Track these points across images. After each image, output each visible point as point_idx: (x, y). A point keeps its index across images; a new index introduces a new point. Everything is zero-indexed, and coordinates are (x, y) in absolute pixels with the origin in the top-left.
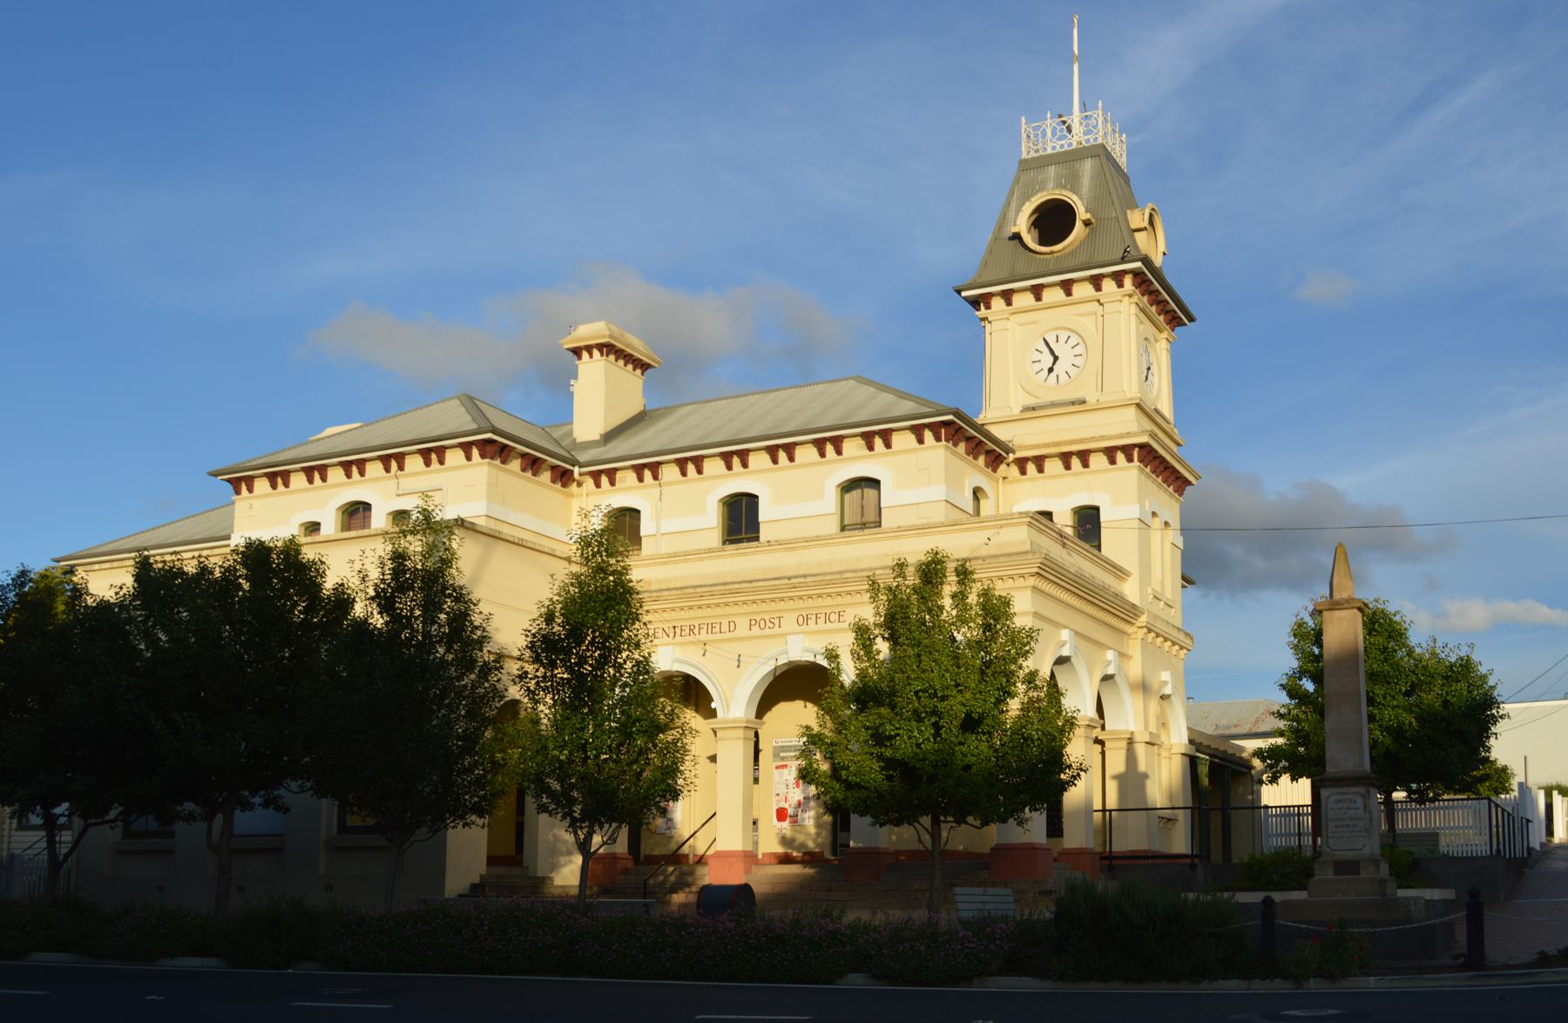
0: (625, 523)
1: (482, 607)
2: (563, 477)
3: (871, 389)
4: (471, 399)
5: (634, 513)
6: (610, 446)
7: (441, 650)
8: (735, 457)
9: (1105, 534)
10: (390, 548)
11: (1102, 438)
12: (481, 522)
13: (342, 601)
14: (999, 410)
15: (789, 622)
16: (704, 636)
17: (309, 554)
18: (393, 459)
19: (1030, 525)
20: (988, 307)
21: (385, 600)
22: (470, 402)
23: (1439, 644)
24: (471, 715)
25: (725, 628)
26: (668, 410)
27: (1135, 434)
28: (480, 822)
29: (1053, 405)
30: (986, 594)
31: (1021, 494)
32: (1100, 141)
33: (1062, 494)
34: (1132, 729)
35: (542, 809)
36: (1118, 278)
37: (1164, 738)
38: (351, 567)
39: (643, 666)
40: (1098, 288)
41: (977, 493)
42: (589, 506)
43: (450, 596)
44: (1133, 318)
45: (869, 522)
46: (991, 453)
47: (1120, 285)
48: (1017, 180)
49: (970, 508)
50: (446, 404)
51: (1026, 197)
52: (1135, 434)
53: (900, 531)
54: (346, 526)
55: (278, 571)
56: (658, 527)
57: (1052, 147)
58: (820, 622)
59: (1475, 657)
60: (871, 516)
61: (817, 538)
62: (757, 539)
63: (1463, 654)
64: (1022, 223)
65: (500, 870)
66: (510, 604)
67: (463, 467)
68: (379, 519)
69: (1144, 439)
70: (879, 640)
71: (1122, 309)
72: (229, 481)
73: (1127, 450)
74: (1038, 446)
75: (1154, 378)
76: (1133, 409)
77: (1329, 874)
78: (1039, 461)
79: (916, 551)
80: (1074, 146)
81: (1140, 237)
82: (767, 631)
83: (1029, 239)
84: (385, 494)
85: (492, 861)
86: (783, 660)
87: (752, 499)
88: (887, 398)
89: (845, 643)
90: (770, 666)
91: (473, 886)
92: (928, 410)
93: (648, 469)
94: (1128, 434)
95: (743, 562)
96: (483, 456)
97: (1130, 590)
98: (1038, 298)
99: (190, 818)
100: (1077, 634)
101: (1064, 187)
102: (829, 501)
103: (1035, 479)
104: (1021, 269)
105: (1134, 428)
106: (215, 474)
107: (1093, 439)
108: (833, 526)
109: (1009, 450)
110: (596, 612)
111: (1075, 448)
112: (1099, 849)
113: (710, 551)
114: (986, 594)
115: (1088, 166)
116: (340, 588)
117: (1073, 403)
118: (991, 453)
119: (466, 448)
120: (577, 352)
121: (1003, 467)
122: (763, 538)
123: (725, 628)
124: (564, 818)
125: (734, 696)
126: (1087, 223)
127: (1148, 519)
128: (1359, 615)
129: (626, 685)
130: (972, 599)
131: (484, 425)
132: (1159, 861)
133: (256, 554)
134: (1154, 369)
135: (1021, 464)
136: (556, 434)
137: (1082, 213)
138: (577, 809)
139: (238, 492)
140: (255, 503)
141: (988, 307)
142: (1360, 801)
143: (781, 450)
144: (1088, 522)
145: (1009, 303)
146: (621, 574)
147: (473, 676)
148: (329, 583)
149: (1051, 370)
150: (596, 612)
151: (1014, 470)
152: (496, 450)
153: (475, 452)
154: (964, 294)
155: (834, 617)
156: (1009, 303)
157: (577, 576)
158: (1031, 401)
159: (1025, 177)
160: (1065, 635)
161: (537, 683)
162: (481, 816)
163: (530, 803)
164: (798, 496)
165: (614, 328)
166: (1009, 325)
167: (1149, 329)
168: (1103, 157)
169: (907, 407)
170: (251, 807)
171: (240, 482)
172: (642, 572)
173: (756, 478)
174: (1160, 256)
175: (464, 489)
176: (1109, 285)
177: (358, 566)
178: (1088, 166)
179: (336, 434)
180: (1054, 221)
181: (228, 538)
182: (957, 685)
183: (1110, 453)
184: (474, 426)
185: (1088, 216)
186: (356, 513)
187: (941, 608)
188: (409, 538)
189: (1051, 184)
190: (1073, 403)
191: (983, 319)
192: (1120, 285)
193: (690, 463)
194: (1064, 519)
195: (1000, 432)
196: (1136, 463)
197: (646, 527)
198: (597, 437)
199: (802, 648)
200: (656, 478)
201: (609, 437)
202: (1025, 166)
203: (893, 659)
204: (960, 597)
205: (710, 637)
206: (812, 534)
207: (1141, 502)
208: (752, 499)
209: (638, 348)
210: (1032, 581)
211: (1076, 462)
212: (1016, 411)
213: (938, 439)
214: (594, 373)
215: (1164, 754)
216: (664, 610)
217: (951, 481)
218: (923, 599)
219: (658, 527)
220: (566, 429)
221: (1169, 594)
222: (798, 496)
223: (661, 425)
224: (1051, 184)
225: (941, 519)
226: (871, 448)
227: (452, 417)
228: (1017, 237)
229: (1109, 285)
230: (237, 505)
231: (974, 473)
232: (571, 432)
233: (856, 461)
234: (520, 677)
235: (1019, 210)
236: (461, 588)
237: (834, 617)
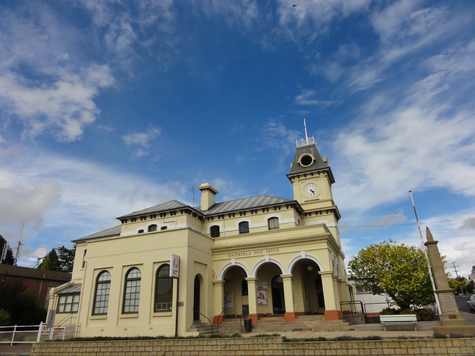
6: (210, 211)
25: (248, 254)
29: (312, 200)
56: (224, 230)
57: (303, 145)
62: (248, 232)
77: (448, 319)
93: (221, 216)
102: (237, 227)
104: (301, 171)
112: (339, 309)
120: (202, 190)
122: (251, 231)
123: (248, 254)
137: (313, 158)
143: (254, 210)
181: (119, 234)
183: (327, 211)
193: (232, 214)
197: (221, 230)
201: (210, 209)
202: (298, 149)
214: (206, 195)
219: (224, 230)
228: (299, 164)
233: (243, 219)
237: (276, 250)
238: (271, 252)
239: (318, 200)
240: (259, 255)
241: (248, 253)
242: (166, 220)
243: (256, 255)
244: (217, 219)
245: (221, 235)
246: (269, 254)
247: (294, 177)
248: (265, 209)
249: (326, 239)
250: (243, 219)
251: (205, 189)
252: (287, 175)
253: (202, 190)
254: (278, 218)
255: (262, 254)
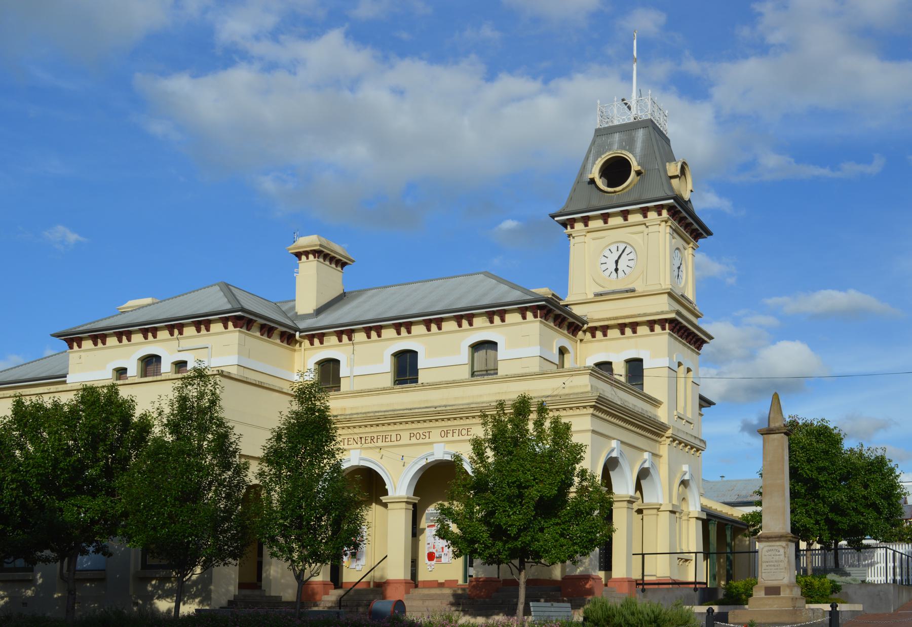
0: (329, 370)
1: (235, 431)
2: (288, 338)
3: (494, 281)
4: (227, 285)
5: (336, 362)
7: (210, 457)
8: (403, 325)
9: (646, 380)
10: (177, 394)
11: (645, 315)
12: (234, 371)
13: (145, 426)
14: (579, 293)
15: (435, 435)
16: (380, 444)
17: (124, 393)
18: (175, 326)
19: (591, 374)
20: (572, 227)
21: (174, 427)
22: (227, 288)
23: (865, 448)
24: (228, 497)
25: (394, 438)
26: (360, 292)
27: (667, 313)
28: (234, 562)
29: (614, 292)
30: (556, 421)
31: (591, 351)
32: (649, 117)
33: (617, 351)
34: (660, 502)
35: (273, 555)
36: (658, 210)
37: (684, 507)
38: (152, 401)
39: (337, 468)
40: (645, 216)
41: (562, 351)
42: (303, 363)
43: (216, 423)
44: (668, 235)
45: (490, 372)
46: (570, 324)
47: (660, 214)
48: (594, 142)
49: (556, 361)
50: (210, 289)
51: (598, 155)
52: (667, 313)
53: (508, 378)
54: (144, 373)
55: (103, 410)
56: (351, 371)
58: (456, 435)
59: (887, 457)
60: (491, 366)
61: (454, 382)
62: (415, 381)
63: (878, 454)
64: (595, 172)
65: (247, 592)
66: (255, 426)
67: (221, 333)
68: (166, 366)
69: (673, 315)
70: (488, 450)
71: (656, 235)
72: (65, 340)
73: (662, 323)
74: (603, 320)
75: (683, 275)
76: (666, 296)
77: (762, 594)
78: (605, 329)
79: (510, 392)
80: (632, 120)
81: (675, 182)
82: (421, 441)
83: (600, 183)
84: (167, 348)
85: (242, 586)
86: (430, 460)
87: (413, 354)
88: (504, 288)
89: (466, 452)
90: (423, 463)
91: (229, 602)
92: (529, 297)
93: (345, 332)
94: (662, 313)
95: (407, 398)
96: (235, 326)
97: (662, 415)
98: (606, 222)
99: (47, 560)
100: (622, 442)
101: (624, 149)
102: (464, 355)
103: (601, 341)
104: (595, 203)
105: (666, 308)
106: (58, 336)
107: (639, 316)
108: (465, 373)
109: (584, 323)
110: (310, 430)
111: (627, 321)
113: (384, 389)
114: (556, 421)
115: (640, 134)
116: (144, 417)
117: (627, 291)
118: (570, 324)
119: (225, 321)
120: (298, 255)
121: (580, 333)
122: (420, 381)
123: (394, 438)
124: (287, 560)
125: (400, 485)
126: (638, 173)
127: (675, 367)
128: (786, 438)
129: (326, 480)
130: (547, 424)
131: (237, 306)
132: (661, 586)
133: (89, 394)
134: (683, 268)
135: (593, 331)
136: (285, 307)
137: (635, 166)
138: (295, 555)
139: (71, 347)
140: (82, 354)
141: (572, 227)
142: (782, 551)
143: (433, 321)
144: (635, 367)
145: (586, 225)
146: (323, 411)
147: (230, 473)
148: (138, 413)
149: (616, 270)
150: (310, 430)
151: (588, 335)
152: (243, 320)
153: (230, 324)
154: (556, 219)
155: (464, 432)
156: (586, 225)
157: (296, 413)
158: (600, 290)
159: (599, 140)
160: (614, 444)
161: (271, 478)
162: (235, 559)
163: (266, 551)
164: (443, 352)
165: (323, 239)
166: (586, 239)
167: (679, 242)
168: (651, 128)
169: (516, 295)
170: (87, 553)
171: (73, 339)
172: (336, 405)
173: (416, 340)
174: (688, 192)
175: (221, 350)
176: (652, 215)
177: (156, 405)
178: (640, 134)
179: (138, 306)
180: (616, 170)
182: (534, 480)
183: (651, 324)
184: (229, 307)
185: (639, 168)
186: (150, 363)
187: (527, 431)
188: (189, 387)
189: (616, 146)
190: (627, 291)
191: (569, 235)
192: (660, 214)
193: (373, 328)
194: (620, 370)
195: (577, 311)
196: (667, 331)
197: (344, 371)
198: (312, 312)
199: (441, 452)
200: (350, 339)
201: (319, 311)
203: (497, 463)
204: (539, 424)
205: (384, 444)
206: (451, 379)
207: (670, 356)
208: (413, 354)
209: (338, 249)
210: (591, 411)
211: (628, 331)
212: (591, 296)
213: (535, 316)
214: (309, 268)
215: (684, 518)
216: (354, 427)
217: (544, 343)
218: (516, 426)
219: (351, 371)
220: (291, 304)
221: (689, 415)
222: (443, 352)
223: (354, 303)
224: (616, 146)
225: (536, 369)
226: (492, 322)
227: (213, 300)
228: (592, 181)
229: (652, 215)
230: (71, 355)
231: (560, 338)
232: (294, 308)
233: (482, 330)
234: (260, 474)
235: (594, 163)
236: (222, 419)
237: (464, 432)
238: (450, 435)
239: (633, 291)
240: (421, 441)
241: (394, 435)
242: (185, 343)
243: (414, 440)
244: (334, 339)
245: (345, 385)
246: (445, 439)
247: (571, 223)
248: (464, 316)
249: (591, 407)
250: (405, 343)
251: (307, 253)
252: (553, 217)
253: (298, 255)
254: (495, 344)
255: (427, 440)
